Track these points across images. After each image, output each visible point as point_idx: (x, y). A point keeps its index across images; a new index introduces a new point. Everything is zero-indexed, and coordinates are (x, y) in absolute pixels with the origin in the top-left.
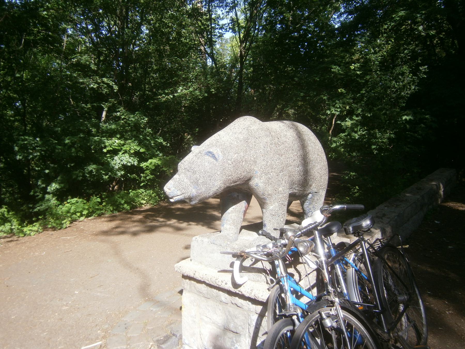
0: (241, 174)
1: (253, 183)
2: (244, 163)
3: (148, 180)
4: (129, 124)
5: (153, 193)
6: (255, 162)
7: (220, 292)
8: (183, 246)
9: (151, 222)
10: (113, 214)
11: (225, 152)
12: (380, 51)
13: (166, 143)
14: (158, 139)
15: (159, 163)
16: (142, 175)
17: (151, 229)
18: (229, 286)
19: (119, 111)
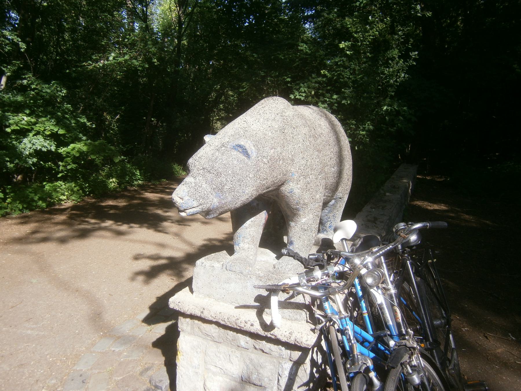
0: (277, 176)
1: (285, 189)
2: (281, 162)
3: (68, 171)
4: (42, 96)
5: (75, 187)
6: (293, 160)
7: (239, 334)
8: (130, 256)
9: (80, 224)
10: (23, 214)
11: (259, 146)
12: (371, 29)
13: (91, 124)
14: (81, 118)
15: (85, 149)
16: (60, 163)
17: (84, 234)
18: (257, 328)
19: (25, 79)
